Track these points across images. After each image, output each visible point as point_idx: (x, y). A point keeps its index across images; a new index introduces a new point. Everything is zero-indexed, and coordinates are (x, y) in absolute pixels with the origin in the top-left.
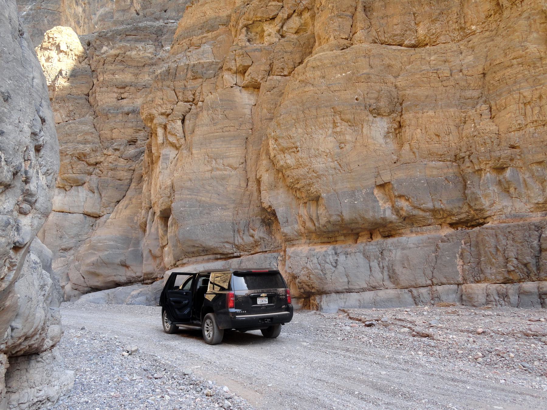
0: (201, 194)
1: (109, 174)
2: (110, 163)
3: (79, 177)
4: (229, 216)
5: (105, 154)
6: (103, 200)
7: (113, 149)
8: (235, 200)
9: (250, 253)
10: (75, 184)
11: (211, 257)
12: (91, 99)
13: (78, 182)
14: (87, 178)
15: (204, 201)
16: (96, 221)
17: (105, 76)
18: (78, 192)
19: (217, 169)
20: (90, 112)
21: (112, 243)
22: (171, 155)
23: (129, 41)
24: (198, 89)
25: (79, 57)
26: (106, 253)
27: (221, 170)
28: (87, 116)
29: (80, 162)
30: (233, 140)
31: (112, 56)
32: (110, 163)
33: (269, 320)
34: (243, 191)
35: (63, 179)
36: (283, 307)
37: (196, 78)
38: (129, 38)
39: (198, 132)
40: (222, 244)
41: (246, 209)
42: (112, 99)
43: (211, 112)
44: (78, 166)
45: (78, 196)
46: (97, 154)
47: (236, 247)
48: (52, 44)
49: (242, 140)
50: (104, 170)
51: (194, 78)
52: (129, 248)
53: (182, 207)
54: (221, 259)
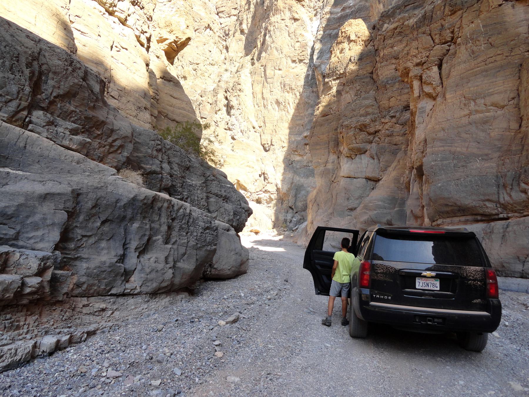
0: (456, 145)
1: (386, 140)
2: (387, 130)
3: (361, 146)
4: (492, 168)
5: (382, 123)
6: (381, 165)
7: (390, 117)
8: (501, 148)
9: (522, 215)
10: (358, 153)
11: (470, 218)
12: (374, 76)
13: (361, 151)
14: (368, 146)
15: (459, 152)
16: (376, 184)
17: (385, 51)
18: (361, 159)
19: (477, 112)
20: (374, 88)
21: (380, 203)
22: (427, 107)
23: (407, 11)
24: (458, 23)
25: (365, 41)
26: (375, 212)
27: (481, 112)
28: (371, 92)
29: (362, 132)
30: (499, 71)
31: (391, 30)
32: (387, 130)
33: (440, 320)
34: (513, 134)
35: (350, 150)
36: (475, 301)
37: (455, 12)
38: (408, 8)
39: (454, 73)
40: (481, 202)
41: (517, 158)
42: (391, 71)
43: (471, 44)
44: (360, 137)
45: (361, 163)
46: (376, 124)
47: (502, 206)
48: (345, 37)
49: (514, 69)
50: (381, 138)
51: (453, 12)
52: (395, 208)
53: (433, 161)
54: (481, 221)
